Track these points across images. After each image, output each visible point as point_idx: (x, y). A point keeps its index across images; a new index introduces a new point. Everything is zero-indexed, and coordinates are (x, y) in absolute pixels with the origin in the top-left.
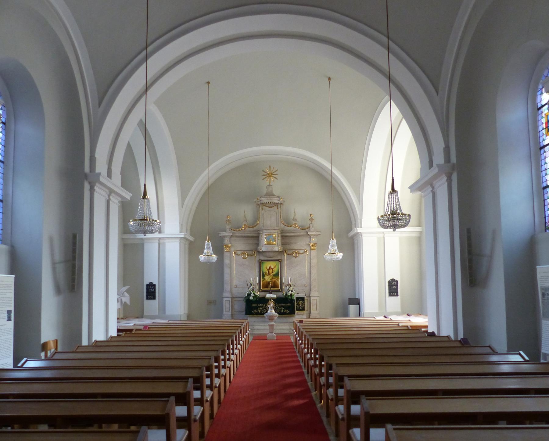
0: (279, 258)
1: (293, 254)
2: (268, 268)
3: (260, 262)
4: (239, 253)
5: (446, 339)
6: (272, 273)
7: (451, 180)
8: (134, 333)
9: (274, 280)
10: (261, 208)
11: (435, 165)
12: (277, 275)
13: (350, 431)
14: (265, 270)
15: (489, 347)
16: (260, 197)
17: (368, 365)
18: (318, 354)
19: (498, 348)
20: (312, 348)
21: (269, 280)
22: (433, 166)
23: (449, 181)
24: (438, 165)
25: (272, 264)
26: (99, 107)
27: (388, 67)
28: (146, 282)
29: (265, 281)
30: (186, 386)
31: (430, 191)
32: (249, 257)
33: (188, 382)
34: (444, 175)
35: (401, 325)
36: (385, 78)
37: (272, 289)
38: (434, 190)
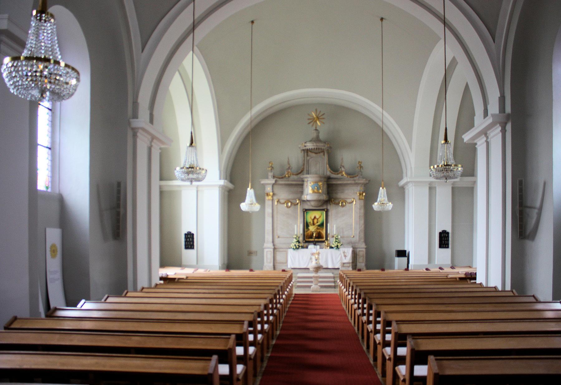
0: (325, 207)
1: (339, 203)
2: (313, 218)
3: (306, 211)
4: (282, 201)
5: (494, 289)
6: (317, 222)
7: (506, 131)
8: (176, 282)
9: (318, 231)
10: (306, 154)
11: (489, 113)
12: (322, 225)
13: (396, 368)
14: (309, 220)
15: (533, 296)
16: (305, 143)
17: (418, 322)
18: (381, 187)
19: (541, 298)
20: (359, 298)
21: (313, 230)
22: (487, 115)
23: (504, 131)
24: (493, 115)
25: (317, 214)
26: (142, 51)
27: (445, 3)
28: (185, 231)
29: (309, 232)
30: (242, 327)
31: (500, 131)
32: (293, 206)
33: (243, 324)
34: (498, 125)
35: (450, 276)
36: (440, 23)
37: (316, 240)
38: (488, 140)
